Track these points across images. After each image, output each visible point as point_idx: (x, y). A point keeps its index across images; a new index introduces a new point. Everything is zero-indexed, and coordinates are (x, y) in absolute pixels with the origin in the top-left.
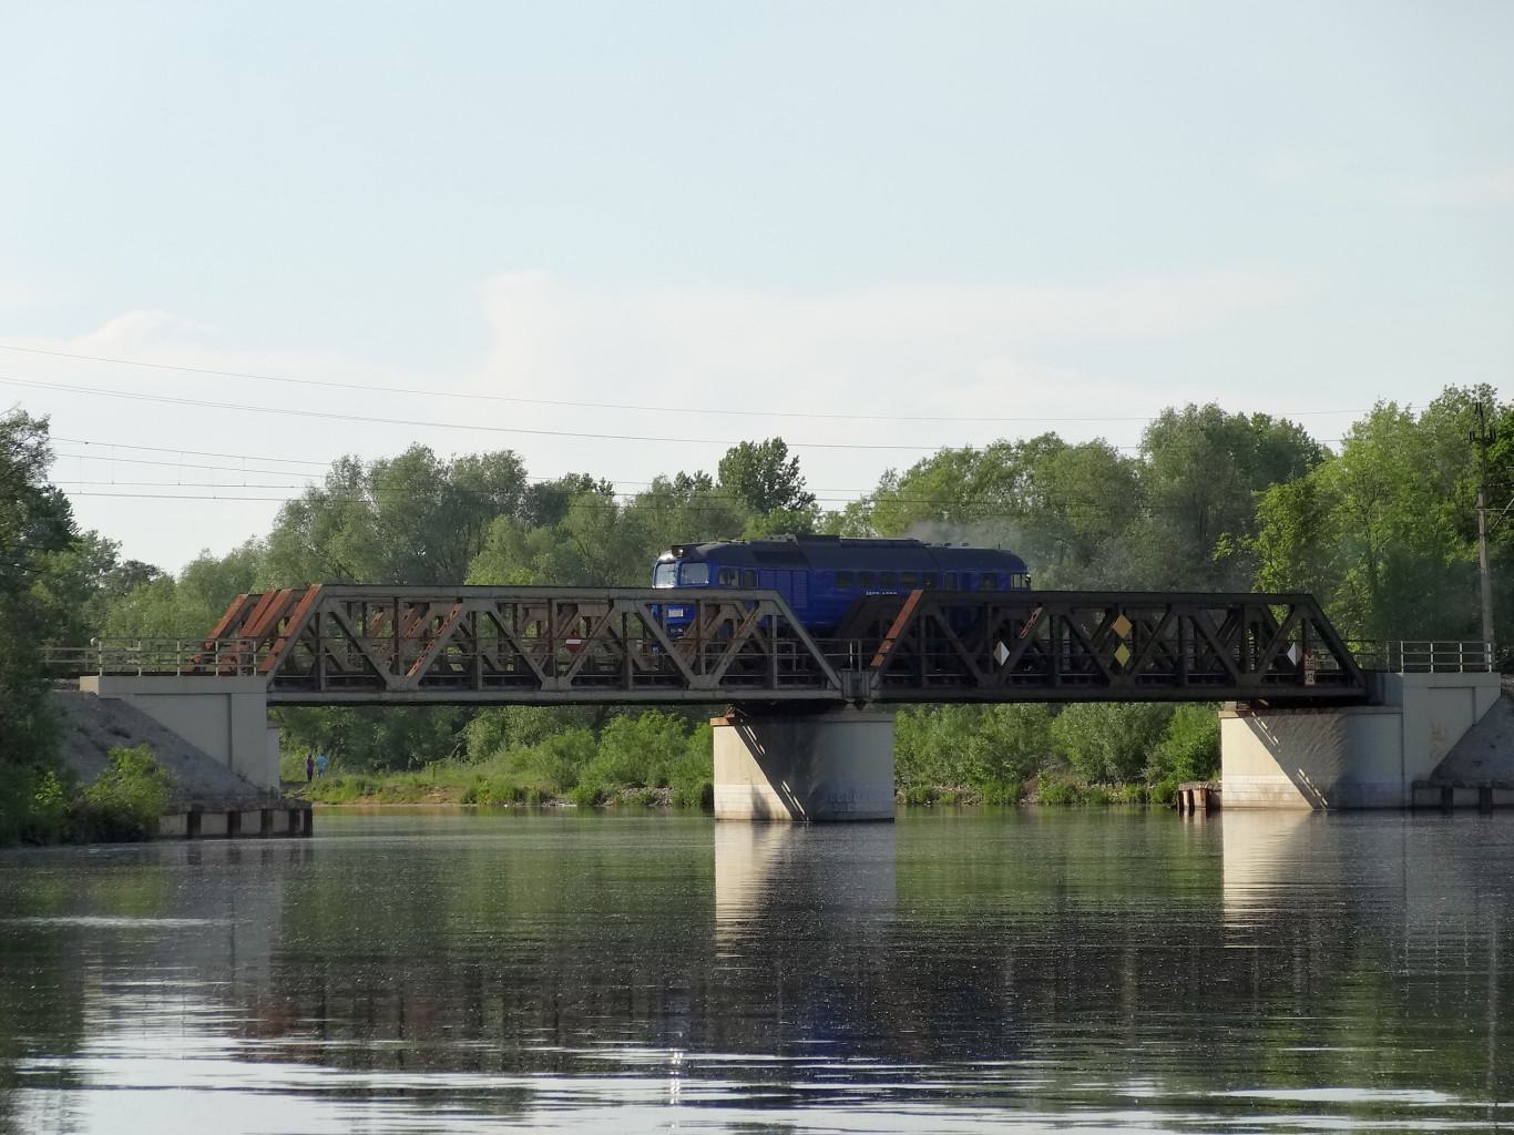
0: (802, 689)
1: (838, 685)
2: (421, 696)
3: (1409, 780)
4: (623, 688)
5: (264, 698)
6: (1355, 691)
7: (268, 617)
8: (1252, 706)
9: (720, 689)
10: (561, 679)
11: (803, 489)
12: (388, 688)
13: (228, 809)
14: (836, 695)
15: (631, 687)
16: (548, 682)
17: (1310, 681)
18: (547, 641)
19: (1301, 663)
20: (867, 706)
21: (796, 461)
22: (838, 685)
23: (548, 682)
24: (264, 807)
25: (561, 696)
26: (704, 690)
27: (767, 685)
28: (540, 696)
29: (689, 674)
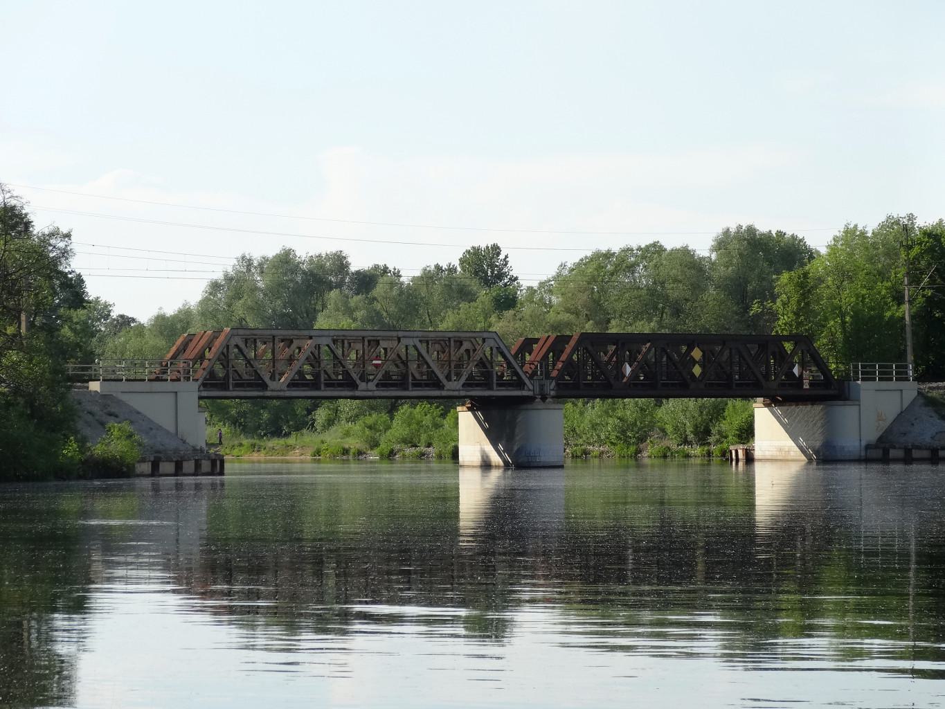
0: (304, 390)
1: (531, 387)
2: (288, 394)
3: (864, 443)
4: (406, 389)
5: (196, 395)
6: (831, 392)
7: (199, 347)
8: (773, 401)
9: (463, 390)
10: (370, 384)
11: (511, 273)
12: (268, 388)
13: (174, 459)
14: (530, 393)
15: (410, 389)
16: (362, 385)
17: (806, 386)
18: (362, 361)
19: (801, 375)
20: (547, 401)
21: (506, 257)
22: (531, 387)
23: (362, 385)
24: (197, 458)
25: (370, 394)
26: (454, 391)
27: (491, 389)
28: (357, 393)
29: (444, 381)
